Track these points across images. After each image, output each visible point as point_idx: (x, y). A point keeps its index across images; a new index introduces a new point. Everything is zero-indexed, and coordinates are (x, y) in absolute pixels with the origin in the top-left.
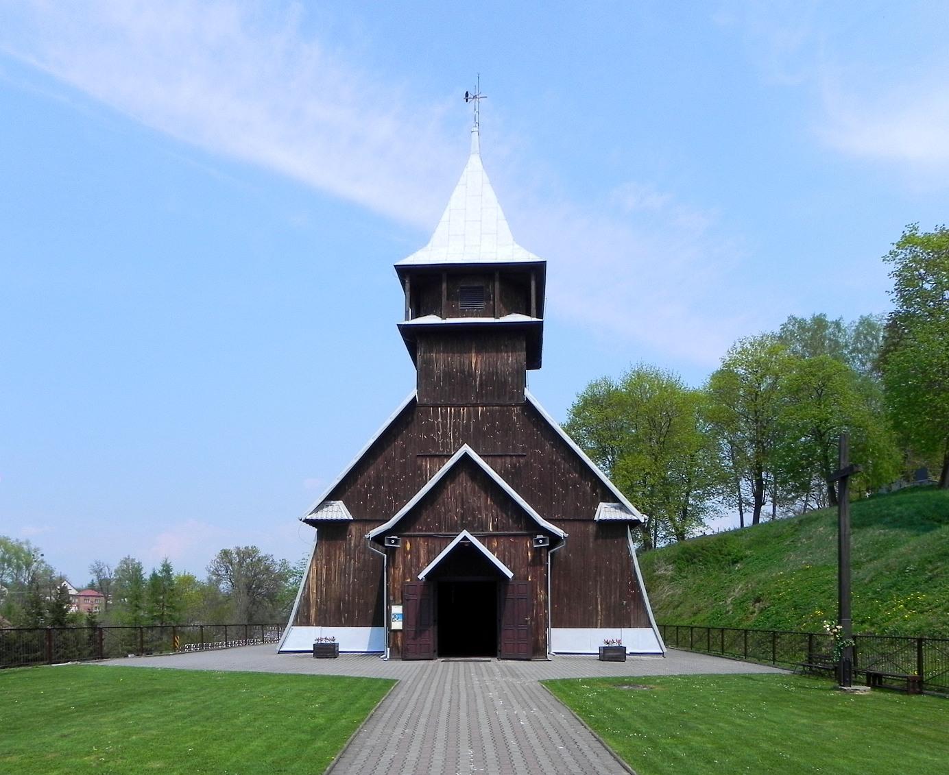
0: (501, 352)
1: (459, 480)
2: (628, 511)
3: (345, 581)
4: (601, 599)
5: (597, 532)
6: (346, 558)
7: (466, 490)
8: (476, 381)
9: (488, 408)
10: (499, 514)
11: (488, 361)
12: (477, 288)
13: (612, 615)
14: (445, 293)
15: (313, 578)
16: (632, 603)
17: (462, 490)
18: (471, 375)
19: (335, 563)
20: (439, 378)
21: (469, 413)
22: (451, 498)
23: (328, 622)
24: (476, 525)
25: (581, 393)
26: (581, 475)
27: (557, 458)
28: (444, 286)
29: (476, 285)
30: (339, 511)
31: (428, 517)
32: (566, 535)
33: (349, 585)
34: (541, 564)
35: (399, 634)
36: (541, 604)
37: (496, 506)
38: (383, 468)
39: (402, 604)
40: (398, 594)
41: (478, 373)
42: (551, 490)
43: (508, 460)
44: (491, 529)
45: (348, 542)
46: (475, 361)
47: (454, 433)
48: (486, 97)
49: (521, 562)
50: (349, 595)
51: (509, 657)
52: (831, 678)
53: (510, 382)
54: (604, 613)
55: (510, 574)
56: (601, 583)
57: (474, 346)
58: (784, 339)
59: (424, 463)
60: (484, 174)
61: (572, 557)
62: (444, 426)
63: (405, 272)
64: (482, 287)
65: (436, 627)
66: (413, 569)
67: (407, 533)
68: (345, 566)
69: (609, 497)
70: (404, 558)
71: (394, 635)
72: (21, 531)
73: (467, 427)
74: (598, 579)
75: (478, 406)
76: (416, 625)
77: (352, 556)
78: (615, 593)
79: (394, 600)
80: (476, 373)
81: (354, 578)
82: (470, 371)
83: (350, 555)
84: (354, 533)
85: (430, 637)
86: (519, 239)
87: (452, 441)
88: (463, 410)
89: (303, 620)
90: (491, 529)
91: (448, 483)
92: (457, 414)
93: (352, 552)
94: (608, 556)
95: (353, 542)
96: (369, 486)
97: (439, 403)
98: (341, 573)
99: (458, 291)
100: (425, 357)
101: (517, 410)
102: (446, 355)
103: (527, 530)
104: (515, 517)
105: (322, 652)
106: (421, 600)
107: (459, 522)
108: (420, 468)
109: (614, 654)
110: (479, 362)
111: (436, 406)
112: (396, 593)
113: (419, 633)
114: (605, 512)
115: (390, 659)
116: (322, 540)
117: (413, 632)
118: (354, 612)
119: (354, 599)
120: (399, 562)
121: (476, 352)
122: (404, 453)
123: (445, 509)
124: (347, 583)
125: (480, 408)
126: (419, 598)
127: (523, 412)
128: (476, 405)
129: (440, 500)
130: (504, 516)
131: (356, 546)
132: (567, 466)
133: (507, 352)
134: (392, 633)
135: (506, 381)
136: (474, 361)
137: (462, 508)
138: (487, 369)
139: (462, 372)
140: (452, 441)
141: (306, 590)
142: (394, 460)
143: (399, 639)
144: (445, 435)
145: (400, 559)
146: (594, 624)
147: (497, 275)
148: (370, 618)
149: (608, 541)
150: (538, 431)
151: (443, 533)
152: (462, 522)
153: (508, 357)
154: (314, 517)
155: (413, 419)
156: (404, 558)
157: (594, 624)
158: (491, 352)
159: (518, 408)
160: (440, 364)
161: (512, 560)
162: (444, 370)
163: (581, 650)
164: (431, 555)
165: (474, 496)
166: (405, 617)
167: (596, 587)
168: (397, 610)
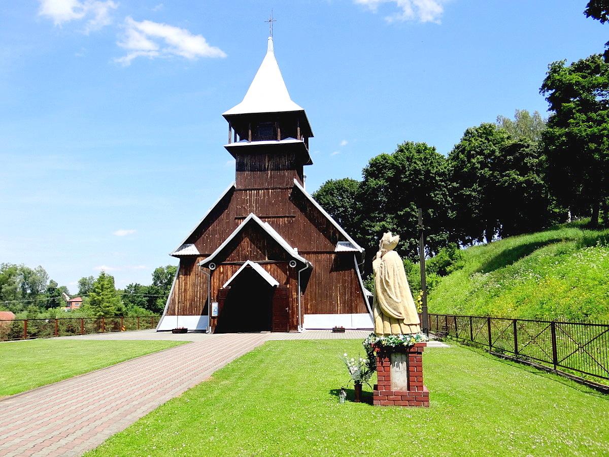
2: (353, 247)
19: (190, 279)
21: (264, 193)
30: (192, 250)
39: (217, 302)
43: (286, 219)
54: (342, 305)
55: (273, 282)
62: (250, 201)
63: (228, 117)
67: (224, 262)
83: (198, 274)
86: (294, 98)
89: (172, 313)
90: (267, 259)
92: (258, 194)
111: (246, 190)
114: (340, 248)
125: (270, 191)
128: (268, 189)
136: (267, 164)
137: (251, 248)
154: (177, 253)
164: (233, 273)
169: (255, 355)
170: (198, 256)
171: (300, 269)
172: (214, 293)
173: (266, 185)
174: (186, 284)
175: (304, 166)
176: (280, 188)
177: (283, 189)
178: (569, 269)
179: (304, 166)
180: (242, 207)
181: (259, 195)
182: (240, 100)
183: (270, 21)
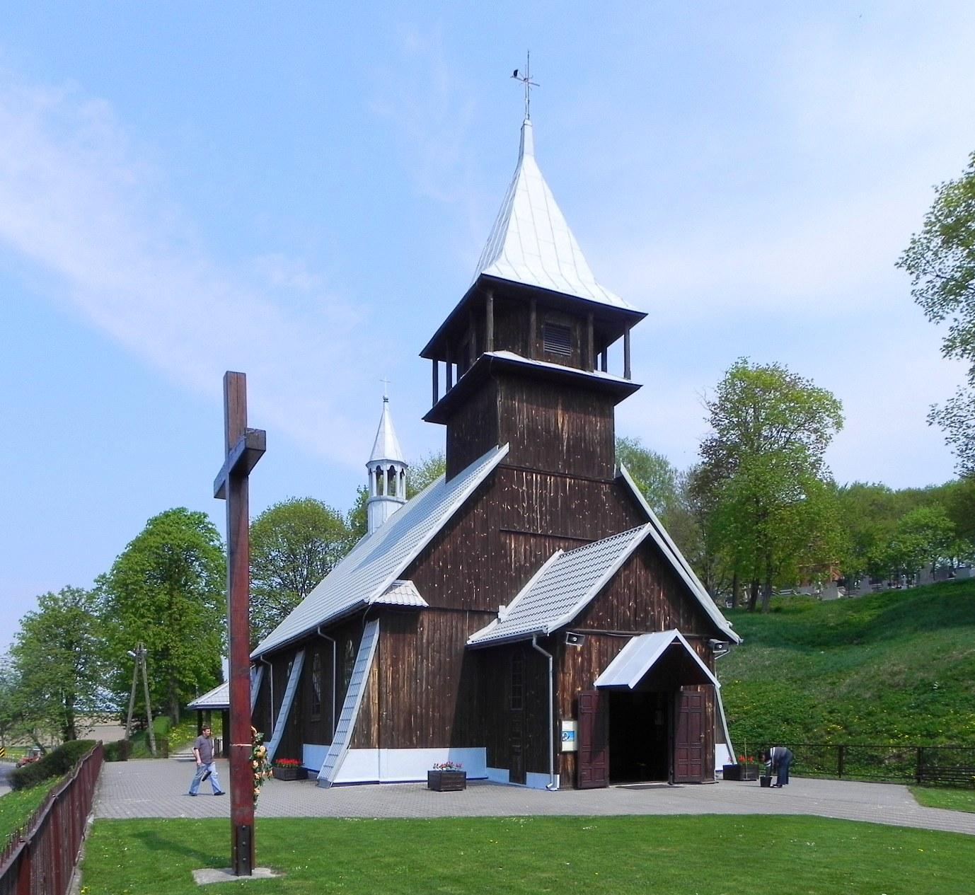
3: (416, 688)
6: (417, 659)
7: (639, 579)
8: (562, 447)
9: (576, 481)
10: (671, 611)
12: (565, 328)
15: (373, 684)
20: (522, 434)
21: (556, 484)
23: (396, 742)
24: (648, 624)
28: (534, 316)
32: (742, 641)
33: (421, 693)
35: (570, 758)
38: (461, 542)
40: (568, 707)
41: (565, 436)
45: (419, 636)
47: (541, 507)
50: (421, 707)
52: (23, 775)
59: (508, 541)
60: (544, 182)
62: (530, 497)
64: (569, 329)
66: (584, 675)
68: (416, 668)
70: (574, 660)
73: (554, 501)
75: (566, 478)
76: (591, 745)
77: (424, 655)
79: (564, 714)
81: (428, 684)
82: (557, 431)
83: (421, 654)
84: (426, 624)
85: (603, 762)
87: (539, 517)
88: (550, 479)
89: (361, 740)
92: (544, 484)
93: (425, 651)
95: (425, 637)
96: (445, 564)
97: (523, 466)
98: (411, 679)
101: (605, 488)
102: (529, 406)
103: (697, 633)
104: (686, 616)
105: (450, 783)
108: (503, 546)
110: (566, 422)
111: (521, 470)
112: (566, 704)
113: (593, 756)
115: (560, 789)
116: (386, 632)
118: (428, 729)
119: (427, 713)
120: (569, 665)
121: (562, 409)
122: (485, 527)
123: (617, 601)
124: (419, 691)
127: (612, 493)
128: (564, 476)
131: (428, 643)
135: (594, 451)
136: (560, 420)
137: (636, 602)
139: (548, 432)
140: (539, 517)
141: (365, 700)
142: (474, 533)
143: (569, 762)
145: (570, 661)
147: (591, 318)
148: (448, 737)
151: (615, 631)
156: (574, 660)
159: (607, 486)
160: (523, 416)
162: (528, 425)
166: (579, 736)
168: (568, 726)
170: (422, 608)
172: (563, 699)
174: (395, 672)
175: (446, 363)
177: (593, 481)
178: (433, 857)
179: (446, 363)
180: (512, 507)
181: (546, 489)
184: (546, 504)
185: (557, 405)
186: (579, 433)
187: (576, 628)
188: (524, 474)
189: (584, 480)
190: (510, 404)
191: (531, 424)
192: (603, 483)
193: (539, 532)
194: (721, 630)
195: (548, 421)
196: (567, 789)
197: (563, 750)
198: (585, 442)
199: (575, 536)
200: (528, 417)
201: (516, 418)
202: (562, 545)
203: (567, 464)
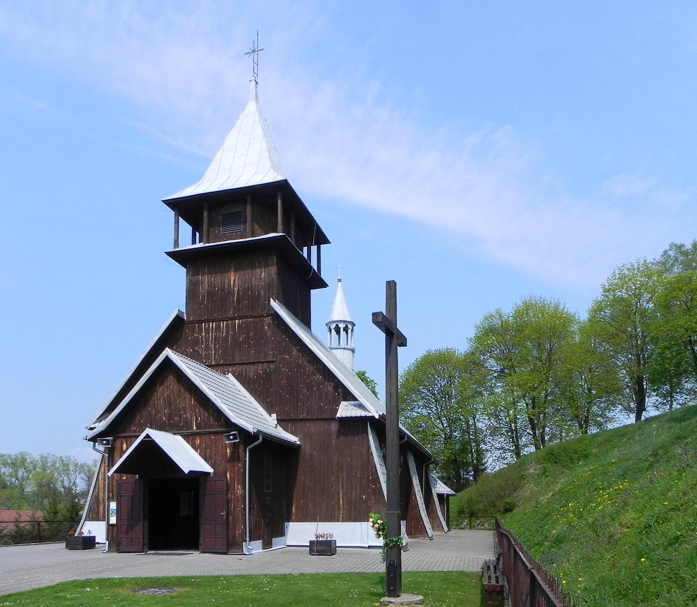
0: (255, 268)
1: (167, 382)
4: (343, 494)
5: (339, 427)
9: (244, 320)
11: (244, 277)
13: (353, 509)
14: (206, 220)
16: (373, 497)
17: (170, 393)
18: (230, 292)
21: (227, 326)
22: (160, 400)
25: (478, 324)
26: (324, 377)
27: (302, 362)
29: (235, 211)
31: (141, 419)
34: (239, 460)
36: (238, 500)
37: (198, 405)
41: (236, 289)
42: (297, 392)
43: (260, 366)
44: (195, 428)
46: (233, 279)
47: (215, 345)
48: (263, 49)
49: (220, 458)
51: (208, 551)
53: (263, 295)
54: (346, 507)
56: (343, 478)
57: (232, 265)
58: (665, 264)
61: (316, 455)
62: (207, 340)
65: (146, 523)
69: (348, 396)
71: (112, 529)
72: (10, 448)
74: (340, 474)
78: (356, 488)
80: (234, 290)
85: (140, 531)
86: (277, 171)
88: (223, 324)
90: (195, 428)
91: (158, 386)
92: (218, 328)
94: (349, 452)
97: (203, 319)
99: (220, 218)
100: (193, 280)
101: (268, 320)
102: (209, 276)
106: (132, 496)
107: (167, 422)
109: (324, 547)
111: (200, 322)
113: (131, 527)
114: (345, 410)
117: (125, 526)
121: (234, 271)
125: (237, 321)
126: (131, 494)
128: (233, 319)
129: (151, 402)
130: (206, 415)
132: (312, 368)
133: (260, 268)
134: (111, 528)
135: (259, 294)
136: (232, 279)
138: (243, 285)
139: (223, 290)
141: (97, 490)
144: (207, 348)
146: (336, 518)
147: (249, 199)
149: (350, 438)
150: (286, 338)
152: (170, 421)
153: (261, 273)
155: (181, 336)
157: (336, 518)
158: (247, 270)
159: (269, 318)
160: (205, 285)
161: (213, 457)
162: (208, 290)
163: (350, 543)
165: (181, 397)
167: (338, 483)
169: (54, 588)
171: (258, 445)
173: (231, 313)
176: (251, 317)
181: (219, 332)
182: (197, 177)
183: (254, 51)
184: (220, 342)
185: (231, 269)
186: (247, 285)
187: (123, 433)
188: (203, 324)
189: (250, 318)
190: (195, 279)
191: (210, 288)
192: (266, 316)
193: (213, 363)
194: (233, 423)
195: (223, 283)
196: (113, 552)
197: (110, 523)
198: (251, 290)
199: (240, 361)
200: (208, 284)
201: (199, 288)
202: (230, 370)
203: (236, 309)
